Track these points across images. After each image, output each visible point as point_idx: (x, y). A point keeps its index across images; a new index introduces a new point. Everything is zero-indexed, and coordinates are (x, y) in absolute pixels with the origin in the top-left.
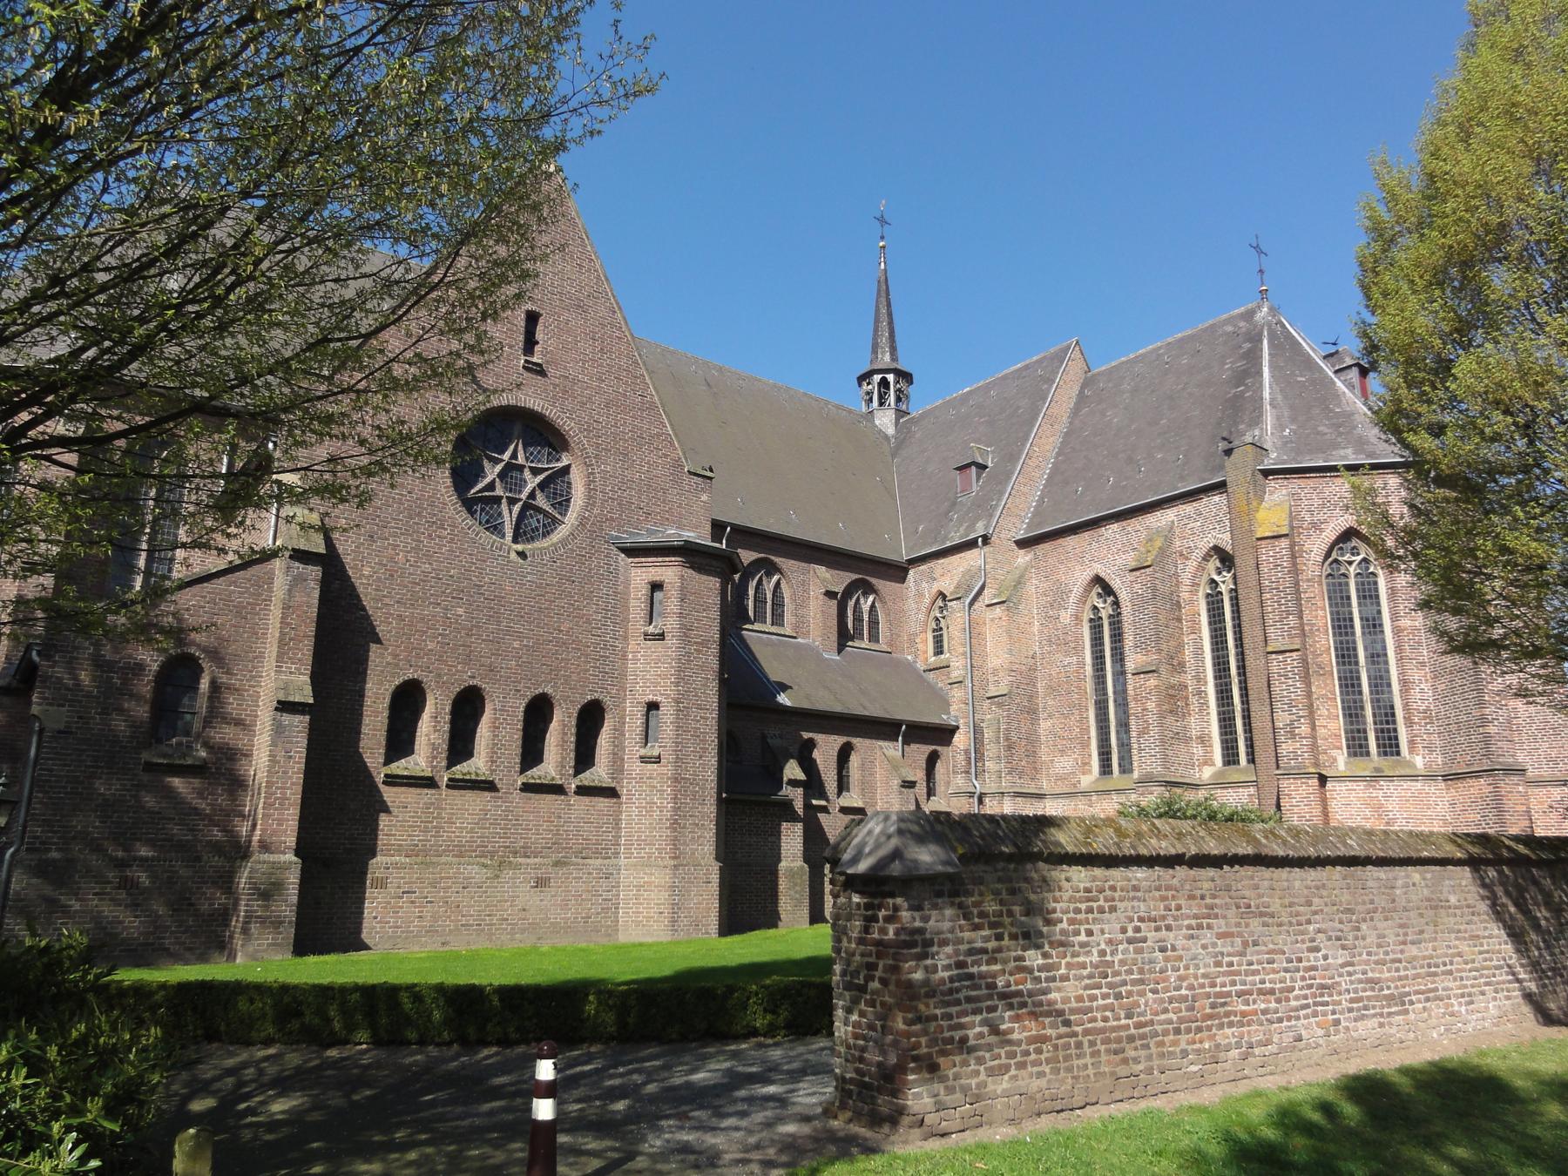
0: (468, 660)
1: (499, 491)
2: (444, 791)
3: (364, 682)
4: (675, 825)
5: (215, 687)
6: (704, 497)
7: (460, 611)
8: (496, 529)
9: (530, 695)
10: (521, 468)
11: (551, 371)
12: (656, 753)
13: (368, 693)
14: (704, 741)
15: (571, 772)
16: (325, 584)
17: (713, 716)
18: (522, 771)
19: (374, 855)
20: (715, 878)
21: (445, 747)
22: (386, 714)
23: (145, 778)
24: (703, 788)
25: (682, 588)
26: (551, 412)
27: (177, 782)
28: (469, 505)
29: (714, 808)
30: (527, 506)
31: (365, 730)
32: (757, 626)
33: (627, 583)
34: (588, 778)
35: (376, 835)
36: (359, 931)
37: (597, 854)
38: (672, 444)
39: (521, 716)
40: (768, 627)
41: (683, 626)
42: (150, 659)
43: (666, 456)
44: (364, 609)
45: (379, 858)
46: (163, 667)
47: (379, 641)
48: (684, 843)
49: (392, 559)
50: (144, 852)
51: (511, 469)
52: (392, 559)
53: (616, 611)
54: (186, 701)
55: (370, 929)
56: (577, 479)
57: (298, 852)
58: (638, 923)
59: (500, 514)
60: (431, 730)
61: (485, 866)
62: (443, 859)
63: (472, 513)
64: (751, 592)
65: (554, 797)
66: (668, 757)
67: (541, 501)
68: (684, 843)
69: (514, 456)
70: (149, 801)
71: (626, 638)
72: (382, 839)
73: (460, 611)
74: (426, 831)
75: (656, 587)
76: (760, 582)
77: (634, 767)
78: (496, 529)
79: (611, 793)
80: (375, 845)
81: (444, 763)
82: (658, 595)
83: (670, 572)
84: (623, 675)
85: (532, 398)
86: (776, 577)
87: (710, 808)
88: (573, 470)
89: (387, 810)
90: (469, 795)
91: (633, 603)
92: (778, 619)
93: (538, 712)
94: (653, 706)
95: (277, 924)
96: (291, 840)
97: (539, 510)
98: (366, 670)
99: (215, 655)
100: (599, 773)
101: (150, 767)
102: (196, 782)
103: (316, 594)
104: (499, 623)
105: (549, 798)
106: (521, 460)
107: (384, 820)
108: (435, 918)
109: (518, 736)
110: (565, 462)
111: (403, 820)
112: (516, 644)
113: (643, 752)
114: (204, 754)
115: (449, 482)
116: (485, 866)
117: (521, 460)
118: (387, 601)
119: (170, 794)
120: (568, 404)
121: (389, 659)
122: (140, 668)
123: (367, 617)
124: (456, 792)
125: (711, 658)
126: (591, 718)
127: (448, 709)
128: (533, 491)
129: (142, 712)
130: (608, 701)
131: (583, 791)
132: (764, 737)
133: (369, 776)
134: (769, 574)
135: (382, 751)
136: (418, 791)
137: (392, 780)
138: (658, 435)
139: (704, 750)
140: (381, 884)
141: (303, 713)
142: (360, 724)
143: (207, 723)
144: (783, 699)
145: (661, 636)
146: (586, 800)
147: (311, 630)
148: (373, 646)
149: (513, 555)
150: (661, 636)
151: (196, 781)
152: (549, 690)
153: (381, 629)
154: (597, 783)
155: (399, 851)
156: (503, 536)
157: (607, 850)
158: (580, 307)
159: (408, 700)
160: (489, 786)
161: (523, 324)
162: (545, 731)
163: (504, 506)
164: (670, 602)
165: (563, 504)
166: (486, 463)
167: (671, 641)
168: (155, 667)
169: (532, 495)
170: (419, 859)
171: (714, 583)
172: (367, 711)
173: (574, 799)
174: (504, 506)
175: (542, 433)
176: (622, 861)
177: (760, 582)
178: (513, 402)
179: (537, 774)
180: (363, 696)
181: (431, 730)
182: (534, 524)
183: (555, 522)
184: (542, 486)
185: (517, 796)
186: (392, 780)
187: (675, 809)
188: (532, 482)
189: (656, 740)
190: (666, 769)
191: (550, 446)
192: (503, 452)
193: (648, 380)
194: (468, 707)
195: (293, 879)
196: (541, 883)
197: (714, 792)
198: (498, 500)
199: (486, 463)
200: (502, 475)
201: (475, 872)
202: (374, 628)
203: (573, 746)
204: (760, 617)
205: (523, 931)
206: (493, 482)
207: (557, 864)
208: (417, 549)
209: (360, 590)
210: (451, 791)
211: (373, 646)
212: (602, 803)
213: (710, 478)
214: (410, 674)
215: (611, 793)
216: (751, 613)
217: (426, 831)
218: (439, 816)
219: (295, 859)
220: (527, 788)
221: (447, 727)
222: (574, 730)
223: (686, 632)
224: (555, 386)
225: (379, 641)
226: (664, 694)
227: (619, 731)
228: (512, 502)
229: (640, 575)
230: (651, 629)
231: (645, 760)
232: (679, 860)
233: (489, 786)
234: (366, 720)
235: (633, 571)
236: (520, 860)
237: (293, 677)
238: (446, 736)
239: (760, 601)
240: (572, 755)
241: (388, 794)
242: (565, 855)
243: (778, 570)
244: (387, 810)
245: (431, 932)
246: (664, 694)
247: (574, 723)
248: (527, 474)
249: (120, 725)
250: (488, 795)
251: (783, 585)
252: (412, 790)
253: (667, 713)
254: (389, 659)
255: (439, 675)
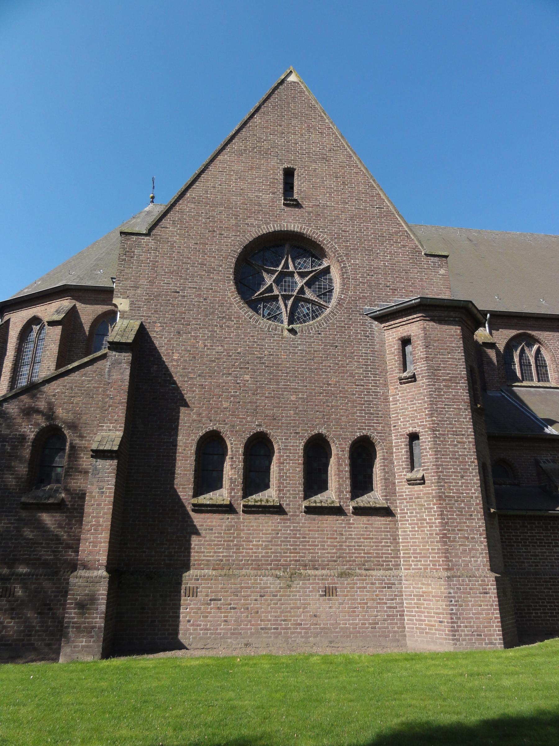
0: (255, 412)
1: (276, 292)
2: (242, 516)
3: (177, 435)
4: (445, 538)
5: (72, 447)
6: (442, 271)
7: (247, 377)
8: (276, 317)
9: (307, 436)
10: (291, 274)
11: (305, 204)
12: (419, 476)
13: (180, 443)
14: (464, 462)
15: (348, 496)
16: (135, 366)
17: (469, 440)
18: (306, 497)
19: (188, 568)
20: (492, 589)
21: (240, 480)
22: (193, 458)
23: (24, 514)
24: (469, 505)
25: (426, 337)
26: (308, 230)
27: (47, 518)
28: (253, 305)
29: (482, 523)
30: (298, 300)
31: (178, 471)
32: (524, 383)
33: (382, 343)
34: (364, 501)
35: (189, 553)
36: (176, 633)
37: (379, 566)
38: (408, 237)
39: (301, 453)
40: (535, 383)
41: (430, 368)
42: (30, 431)
43: (404, 246)
44: (175, 383)
45: (191, 572)
46: (38, 435)
47: (186, 405)
48: (456, 556)
49: (193, 346)
50: (23, 570)
51: (285, 275)
52: (193, 346)
53: (375, 364)
54: (57, 459)
55: (186, 631)
56: (335, 274)
57: (108, 570)
58: (422, 631)
59: (278, 308)
60: (232, 470)
61: (278, 577)
62: (244, 572)
63: (256, 310)
64: (516, 359)
65: (335, 517)
66: (431, 478)
67: (309, 294)
68: (456, 556)
69: (286, 266)
70: (28, 533)
71: (386, 385)
72: (194, 556)
73: (247, 377)
74: (228, 548)
75: (406, 341)
76: (523, 351)
77: (403, 489)
78: (276, 317)
79: (387, 512)
80: (189, 560)
81: (240, 494)
82: (409, 349)
83: (414, 327)
84: (387, 415)
85: (292, 222)
86: (536, 347)
87: (478, 523)
88: (332, 270)
89: (197, 533)
90: (263, 518)
91: (388, 357)
92: (543, 375)
93: (316, 452)
94: (414, 437)
95: (89, 630)
96: (103, 558)
97: (308, 301)
98: (177, 426)
99: (73, 426)
100: (376, 497)
101: (25, 506)
102: (58, 516)
103: (128, 372)
104: (278, 383)
105: (331, 519)
106: (291, 268)
107: (195, 541)
108: (238, 622)
109: (300, 469)
110: (325, 264)
111: (210, 538)
112: (293, 398)
113: (409, 476)
114: (63, 495)
115: (233, 288)
116: (278, 577)
117: (291, 268)
118: (191, 375)
119: (40, 526)
120: (321, 223)
121: (195, 417)
122: (23, 438)
123: (177, 389)
124: (251, 517)
125: (462, 391)
126: (363, 454)
127: (241, 451)
128: (302, 288)
129: (22, 469)
130: (375, 437)
131: (359, 511)
132: (537, 463)
133: (183, 506)
134: (530, 345)
135: (191, 486)
136: (221, 516)
137: (200, 509)
138: (396, 233)
139: (465, 470)
140: (193, 592)
141: (112, 458)
142: (174, 466)
143: (68, 474)
144: (550, 430)
145: (413, 378)
146: (364, 519)
147: (123, 398)
148: (182, 409)
149: (286, 333)
150: (413, 378)
151: (58, 515)
152: (323, 431)
153: (188, 396)
154: (372, 504)
155: (208, 565)
156: (282, 322)
157: (390, 562)
158: (325, 159)
159: (211, 448)
160: (278, 510)
161: (282, 177)
162: (327, 464)
163: (281, 302)
164: (417, 351)
165: (327, 293)
166: (265, 275)
167: (422, 381)
168: (32, 436)
169: (302, 291)
170: (223, 572)
171: (455, 331)
172: (179, 457)
173: (353, 519)
174: (281, 302)
175: (305, 247)
176: (403, 572)
177: (523, 351)
178: (278, 228)
179: (320, 499)
180: (176, 445)
181: (232, 470)
182: (305, 311)
183: (322, 307)
184: (309, 284)
185: (303, 518)
186: (200, 509)
187: (444, 525)
188: (300, 282)
189: (420, 466)
190: (430, 489)
191: (313, 256)
192: (278, 266)
193: (383, 196)
194: (259, 449)
195: (102, 591)
196: (329, 592)
197: (480, 508)
198: (276, 298)
199: (265, 275)
200: (277, 281)
201: (270, 582)
202: (182, 396)
203: (348, 475)
204: (526, 376)
205: (316, 635)
206: (271, 286)
207: (342, 575)
208: (212, 337)
209: (172, 370)
210: (247, 516)
211: (182, 409)
212: (379, 521)
213: (446, 257)
214: (211, 427)
215: (387, 512)
216: (519, 374)
217: (228, 548)
218: (239, 536)
219: (105, 573)
220: (310, 510)
221: (241, 465)
222: (347, 461)
223: (434, 373)
224: (309, 213)
225: (186, 405)
226: (421, 424)
227: (388, 461)
228: (286, 298)
229: (390, 335)
230: (405, 374)
231: (411, 482)
232: (452, 571)
233: (278, 510)
234: (179, 464)
235: (386, 333)
236: (309, 572)
237: (111, 433)
238: (241, 472)
239: (525, 365)
240: (348, 482)
241: (198, 519)
242: (349, 567)
243: (537, 341)
244: (197, 533)
245: (235, 634)
246: (421, 424)
247: (347, 455)
248: (297, 278)
249: (10, 480)
250: (278, 518)
251: (543, 351)
252: (216, 516)
253: (426, 442)
254: (195, 417)
255: (233, 426)
